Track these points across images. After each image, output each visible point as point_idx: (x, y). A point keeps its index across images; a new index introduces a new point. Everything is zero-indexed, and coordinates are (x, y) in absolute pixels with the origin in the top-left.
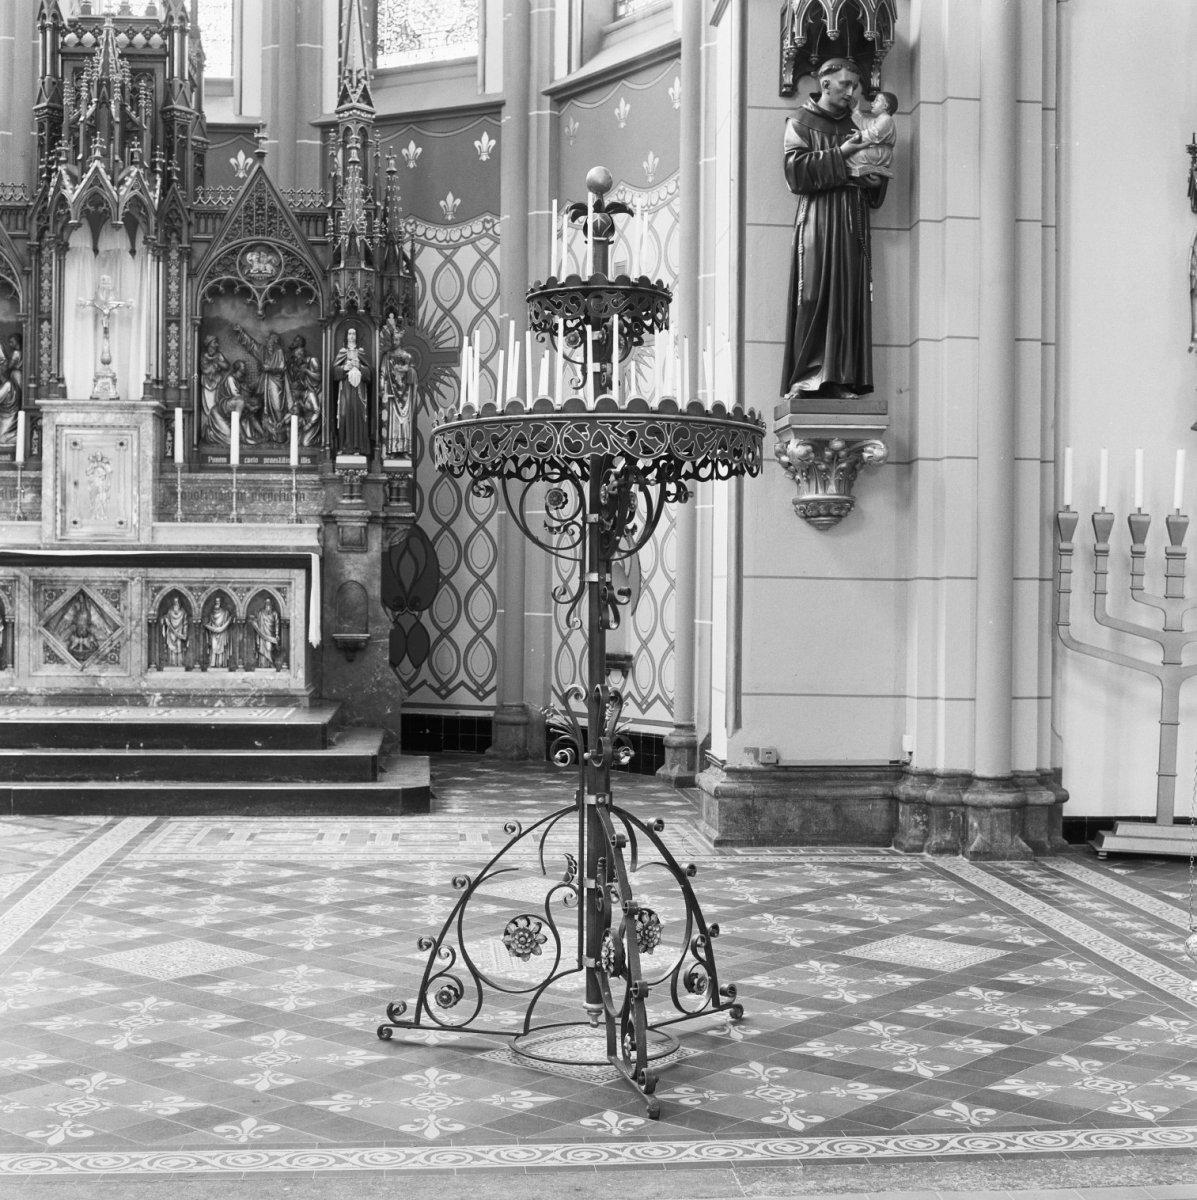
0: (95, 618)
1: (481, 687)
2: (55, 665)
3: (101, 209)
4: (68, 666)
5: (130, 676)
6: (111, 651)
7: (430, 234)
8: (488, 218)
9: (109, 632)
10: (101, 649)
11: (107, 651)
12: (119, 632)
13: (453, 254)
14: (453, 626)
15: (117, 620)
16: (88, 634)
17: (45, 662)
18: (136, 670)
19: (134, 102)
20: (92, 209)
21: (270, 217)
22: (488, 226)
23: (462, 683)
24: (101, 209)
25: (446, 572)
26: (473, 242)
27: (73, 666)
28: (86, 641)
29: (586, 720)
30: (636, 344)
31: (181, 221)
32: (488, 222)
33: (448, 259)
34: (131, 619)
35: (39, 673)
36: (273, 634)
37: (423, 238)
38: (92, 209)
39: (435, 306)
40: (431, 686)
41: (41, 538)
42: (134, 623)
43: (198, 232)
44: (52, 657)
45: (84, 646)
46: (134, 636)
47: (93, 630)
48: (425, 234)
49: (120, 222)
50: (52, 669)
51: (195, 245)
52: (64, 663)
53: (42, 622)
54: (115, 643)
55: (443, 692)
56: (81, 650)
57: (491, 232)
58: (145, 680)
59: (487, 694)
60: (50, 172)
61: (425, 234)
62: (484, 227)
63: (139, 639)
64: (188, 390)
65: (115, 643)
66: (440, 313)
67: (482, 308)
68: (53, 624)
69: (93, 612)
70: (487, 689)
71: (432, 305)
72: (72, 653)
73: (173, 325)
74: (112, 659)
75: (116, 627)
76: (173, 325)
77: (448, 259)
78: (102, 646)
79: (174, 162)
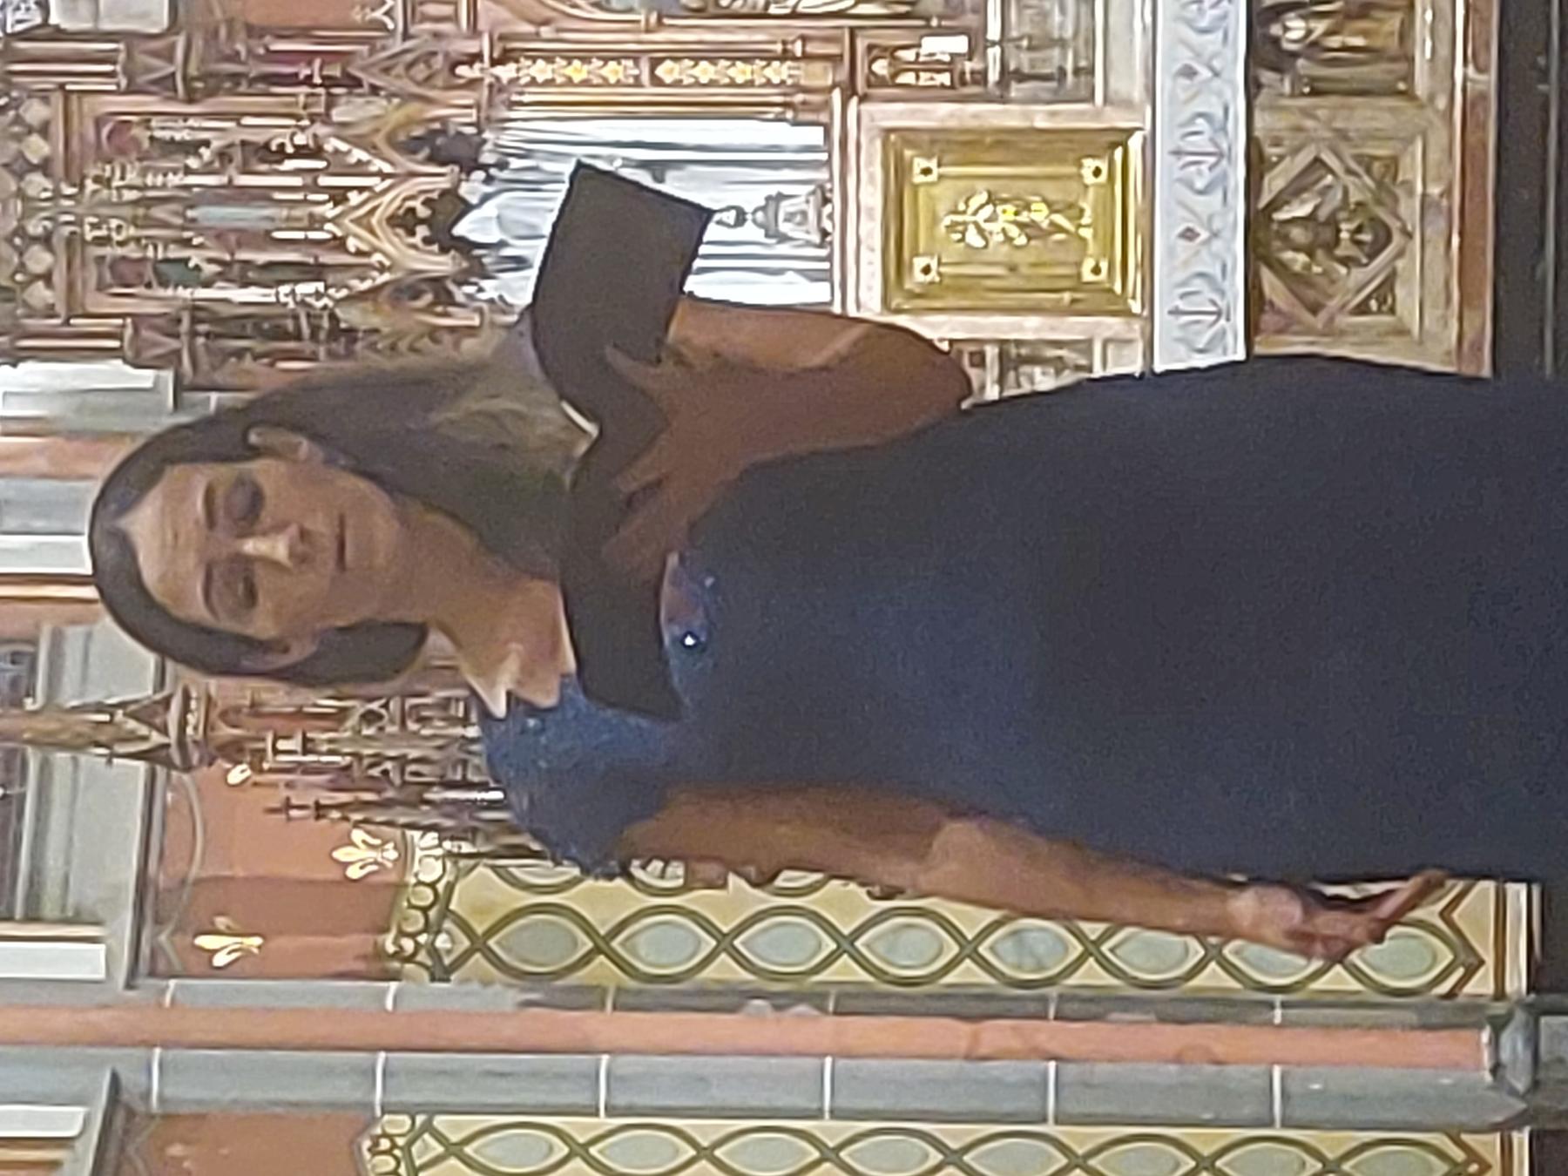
3: (423, 212)
4: (1400, 264)
6: (1368, 171)
8: (367, 1144)
10: (1365, 197)
15: (1304, 158)
16: (1333, 223)
19: (192, 148)
20: (422, 231)
22: (385, 1144)
27: (1400, 254)
29: (1515, 1135)
32: (376, 1144)
37: (432, 913)
38: (422, 231)
41: (1129, 342)
44: (1385, 291)
45: (1359, 230)
46: (1338, 124)
47: (1323, 214)
50: (1407, 298)
51: (483, 25)
54: (1354, 165)
56: (1366, 237)
57: (401, 1141)
58: (1432, 98)
60: (336, 332)
61: (425, 910)
62: (388, 1152)
63: (1345, 113)
64: (804, 39)
65: (1354, 165)
68: (1311, 294)
73: (659, 71)
74: (1387, 175)
76: (659, 71)
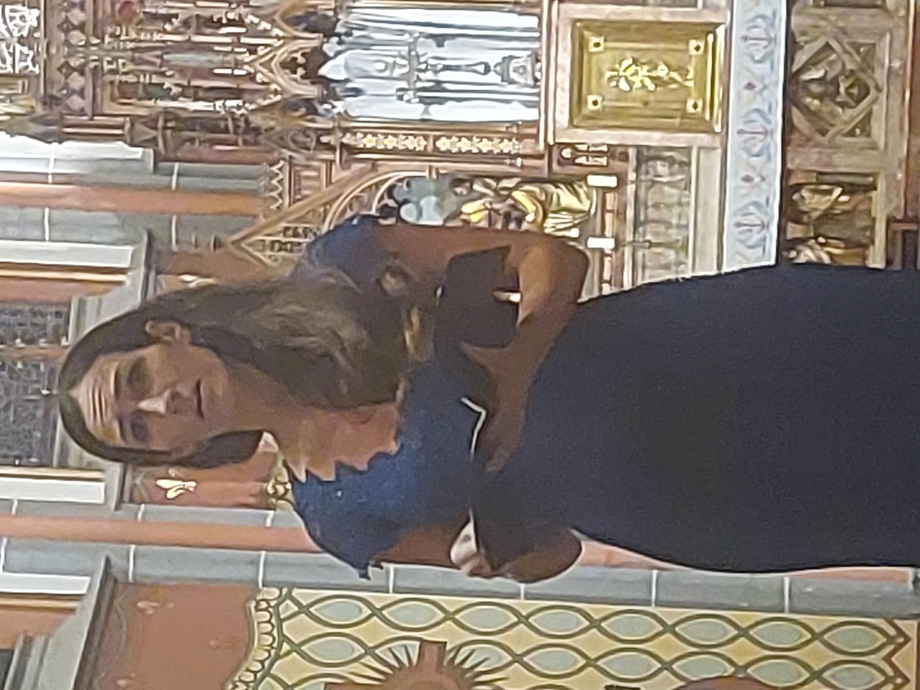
0: (816, 74)
1: (890, 640)
2: (872, 121)
3: (301, 60)
5: (891, 31)
7: (257, 667)
8: (253, 604)
9: (833, 57)
13: (290, 642)
14: (807, 667)
16: (835, 82)
17: (869, 135)
18: (884, 22)
20: (301, 71)
21: (296, 235)
23: (887, 659)
24: (301, 60)
25: (731, 670)
26: (281, 621)
27: (875, 101)
33: (296, 648)
35: (882, 144)
36: (829, 192)
38: (301, 71)
39: (356, 664)
40: (893, 653)
44: (865, 124)
47: (830, 76)
48: (269, 622)
50: (878, 129)
53: (818, 137)
55: (899, 681)
58: (897, 10)
59: (900, 632)
61: (269, 622)
62: (266, 610)
66: (369, 660)
67: (366, 653)
69: (806, 77)
70: (892, 632)
71: (356, 667)
72: (858, 101)
74: (869, 56)
75: (827, 46)
77: (296, 648)
78: (850, 66)
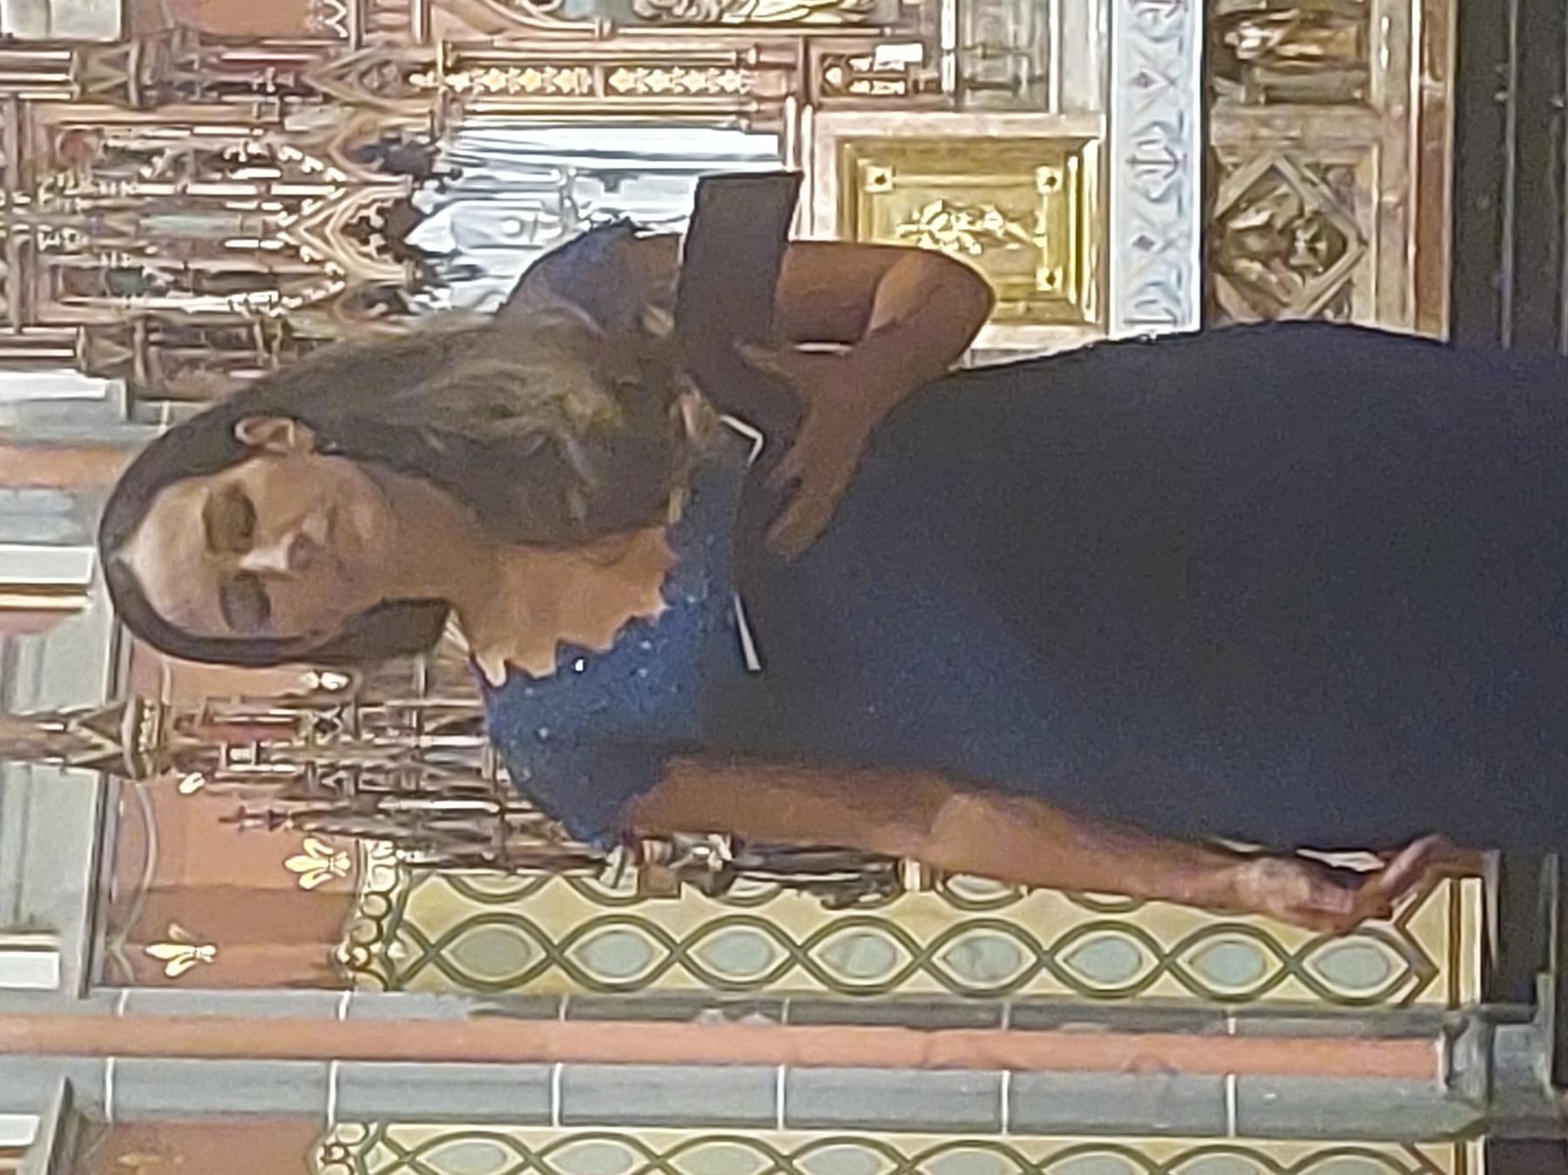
3: (377, 221)
4: (1356, 273)
8: (321, 1152)
11: (1324, 188)
12: (1284, 167)
15: (1260, 166)
16: (1288, 232)
18: (1359, 126)
22: (338, 1153)
28: (1303, 237)
30: (583, 653)
31: (387, 63)
34: (1254, 138)
42: (1264, 132)
43: (408, 27)
46: (1294, 133)
49: (420, 665)
52: (1349, 282)
58: (1388, 106)
62: (341, 1161)
69: (1239, 224)
73: (613, 80)
76: (613, 80)
79: (256, 81)
